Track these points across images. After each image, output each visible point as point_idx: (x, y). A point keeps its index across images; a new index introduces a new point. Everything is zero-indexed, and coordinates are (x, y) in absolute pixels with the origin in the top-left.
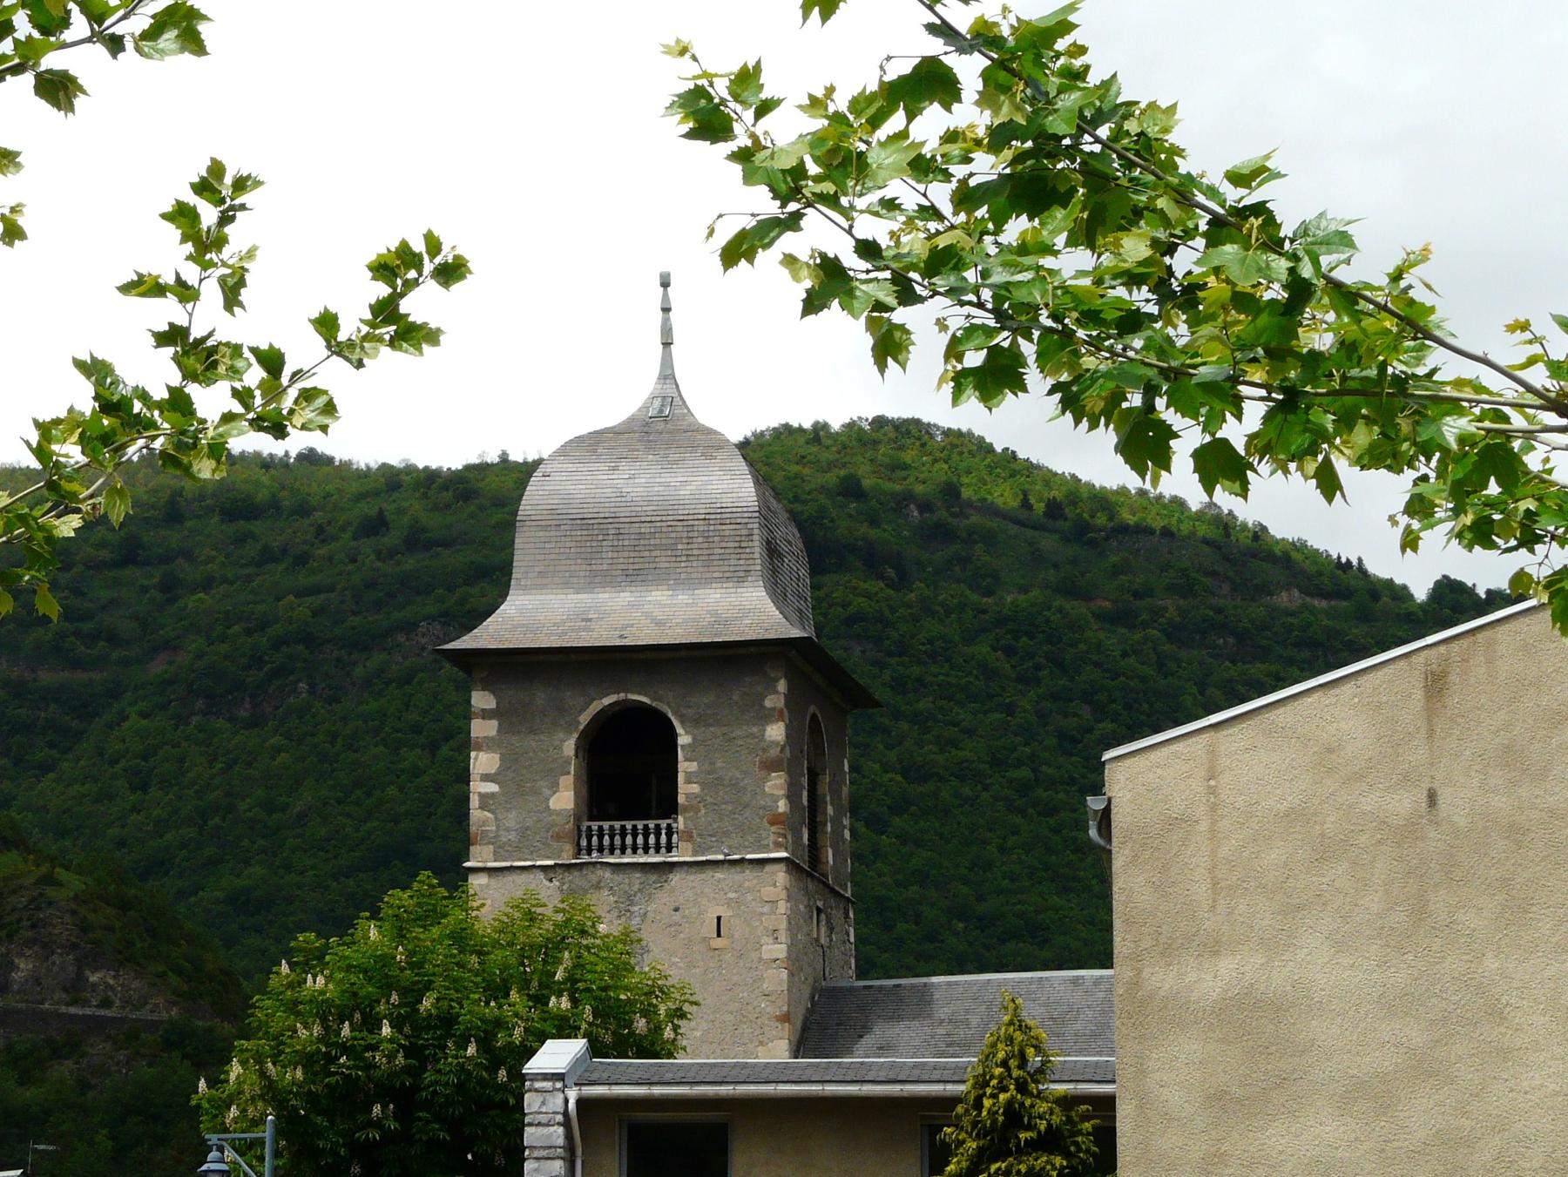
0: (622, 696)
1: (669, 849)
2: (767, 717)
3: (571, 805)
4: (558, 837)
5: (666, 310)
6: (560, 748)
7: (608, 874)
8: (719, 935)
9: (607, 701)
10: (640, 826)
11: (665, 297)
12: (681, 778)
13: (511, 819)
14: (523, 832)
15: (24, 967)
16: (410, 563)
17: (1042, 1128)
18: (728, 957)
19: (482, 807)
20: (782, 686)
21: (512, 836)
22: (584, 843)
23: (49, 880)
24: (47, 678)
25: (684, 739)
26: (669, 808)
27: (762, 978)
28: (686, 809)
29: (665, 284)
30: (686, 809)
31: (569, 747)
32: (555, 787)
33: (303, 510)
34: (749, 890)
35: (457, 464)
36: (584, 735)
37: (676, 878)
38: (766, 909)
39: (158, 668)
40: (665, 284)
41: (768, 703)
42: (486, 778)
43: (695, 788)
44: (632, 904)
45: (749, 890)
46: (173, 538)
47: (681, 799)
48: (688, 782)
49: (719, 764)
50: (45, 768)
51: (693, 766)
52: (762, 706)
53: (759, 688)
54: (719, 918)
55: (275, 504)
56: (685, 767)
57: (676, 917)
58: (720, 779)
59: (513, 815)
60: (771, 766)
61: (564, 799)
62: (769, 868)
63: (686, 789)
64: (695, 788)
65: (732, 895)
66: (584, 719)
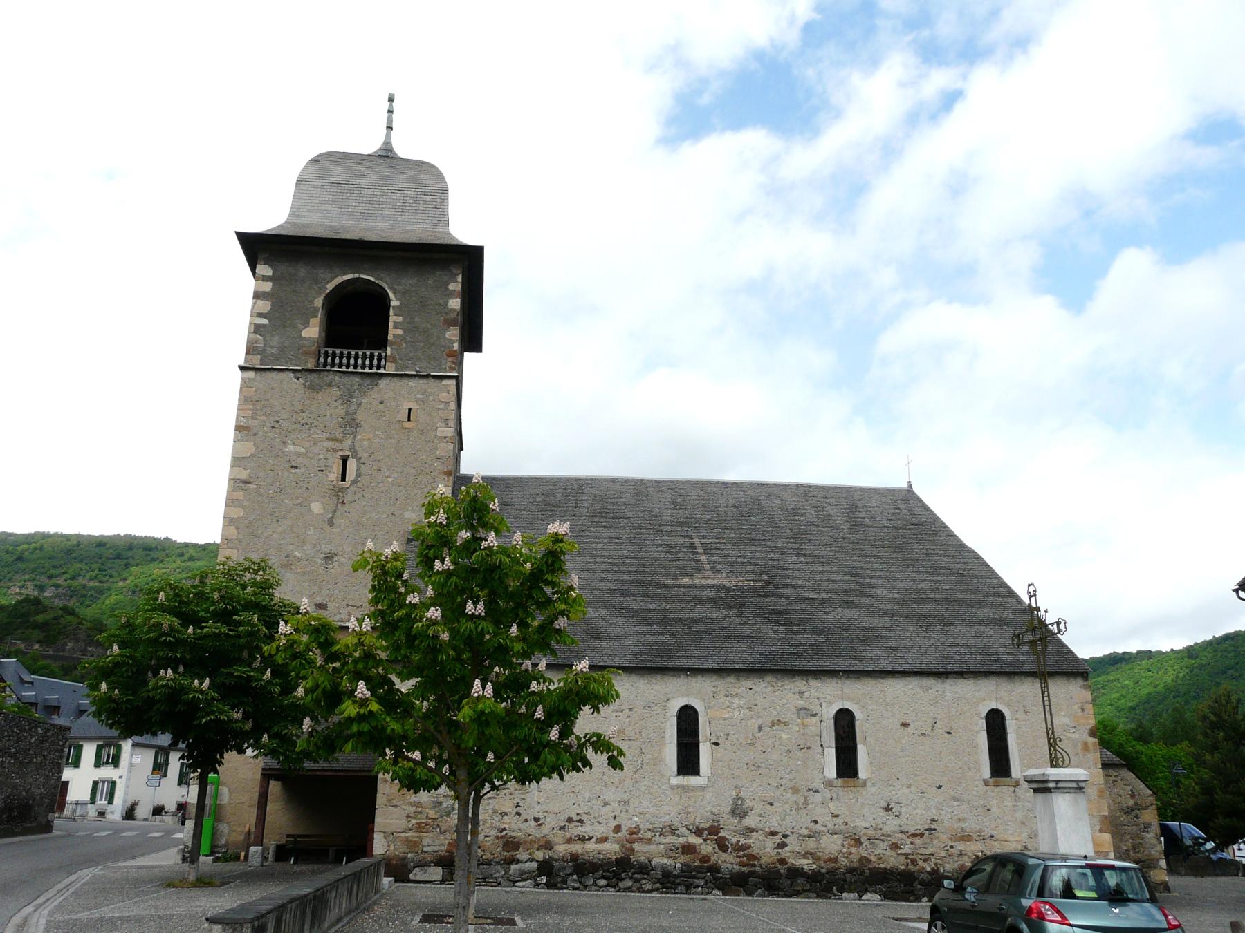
0: (357, 275)
1: (379, 367)
2: (451, 294)
3: (316, 336)
4: (306, 353)
5: (390, 128)
6: (312, 302)
7: (337, 378)
9: (346, 277)
10: (360, 353)
11: (391, 106)
12: (391, 325)
13: (275, 341)
14: (282, 349)
15: (70, 645)
16: (189, 564)
17: (265, 737)
18: (414, 434)
20: (460, 278)
21: (274, 351)
22: (322, 360)
23: (81, 623)
24: (91, 584)
25: (394, 303)
26: (382, 343)
27: (436, 448)
28: (393, 343)
29: (391, 100)
30: (393, 343)
31: (319, 302)
32: (306, 324)
33: (164, 550)
34: (431, 394)
35: (202, 541)
36: (328, 297)
37: (383, 383)
38: (442, 406)
39: (121, 584)
40: (391, 100)
41: (451, 287)
43: (400, 332)
44: (352, 397)
45: (431, 394)
46: (130, 554)
47: (390, 337)
48: (396, 327)
49: (417, 319)
50: (89, 606)
51: (400, 319)
52: (447, 289)
53: (446, 278)
55: (157, 548)
56: (393, 319)
57: (381, 407)
58: (417, 328)
59: (276, 338)
60: (450, 323)
61: (313, 331)
62: (445, 382)
63: (393, 332)
64: (400, 332)
65: (420, 396)
66: (330, 286)
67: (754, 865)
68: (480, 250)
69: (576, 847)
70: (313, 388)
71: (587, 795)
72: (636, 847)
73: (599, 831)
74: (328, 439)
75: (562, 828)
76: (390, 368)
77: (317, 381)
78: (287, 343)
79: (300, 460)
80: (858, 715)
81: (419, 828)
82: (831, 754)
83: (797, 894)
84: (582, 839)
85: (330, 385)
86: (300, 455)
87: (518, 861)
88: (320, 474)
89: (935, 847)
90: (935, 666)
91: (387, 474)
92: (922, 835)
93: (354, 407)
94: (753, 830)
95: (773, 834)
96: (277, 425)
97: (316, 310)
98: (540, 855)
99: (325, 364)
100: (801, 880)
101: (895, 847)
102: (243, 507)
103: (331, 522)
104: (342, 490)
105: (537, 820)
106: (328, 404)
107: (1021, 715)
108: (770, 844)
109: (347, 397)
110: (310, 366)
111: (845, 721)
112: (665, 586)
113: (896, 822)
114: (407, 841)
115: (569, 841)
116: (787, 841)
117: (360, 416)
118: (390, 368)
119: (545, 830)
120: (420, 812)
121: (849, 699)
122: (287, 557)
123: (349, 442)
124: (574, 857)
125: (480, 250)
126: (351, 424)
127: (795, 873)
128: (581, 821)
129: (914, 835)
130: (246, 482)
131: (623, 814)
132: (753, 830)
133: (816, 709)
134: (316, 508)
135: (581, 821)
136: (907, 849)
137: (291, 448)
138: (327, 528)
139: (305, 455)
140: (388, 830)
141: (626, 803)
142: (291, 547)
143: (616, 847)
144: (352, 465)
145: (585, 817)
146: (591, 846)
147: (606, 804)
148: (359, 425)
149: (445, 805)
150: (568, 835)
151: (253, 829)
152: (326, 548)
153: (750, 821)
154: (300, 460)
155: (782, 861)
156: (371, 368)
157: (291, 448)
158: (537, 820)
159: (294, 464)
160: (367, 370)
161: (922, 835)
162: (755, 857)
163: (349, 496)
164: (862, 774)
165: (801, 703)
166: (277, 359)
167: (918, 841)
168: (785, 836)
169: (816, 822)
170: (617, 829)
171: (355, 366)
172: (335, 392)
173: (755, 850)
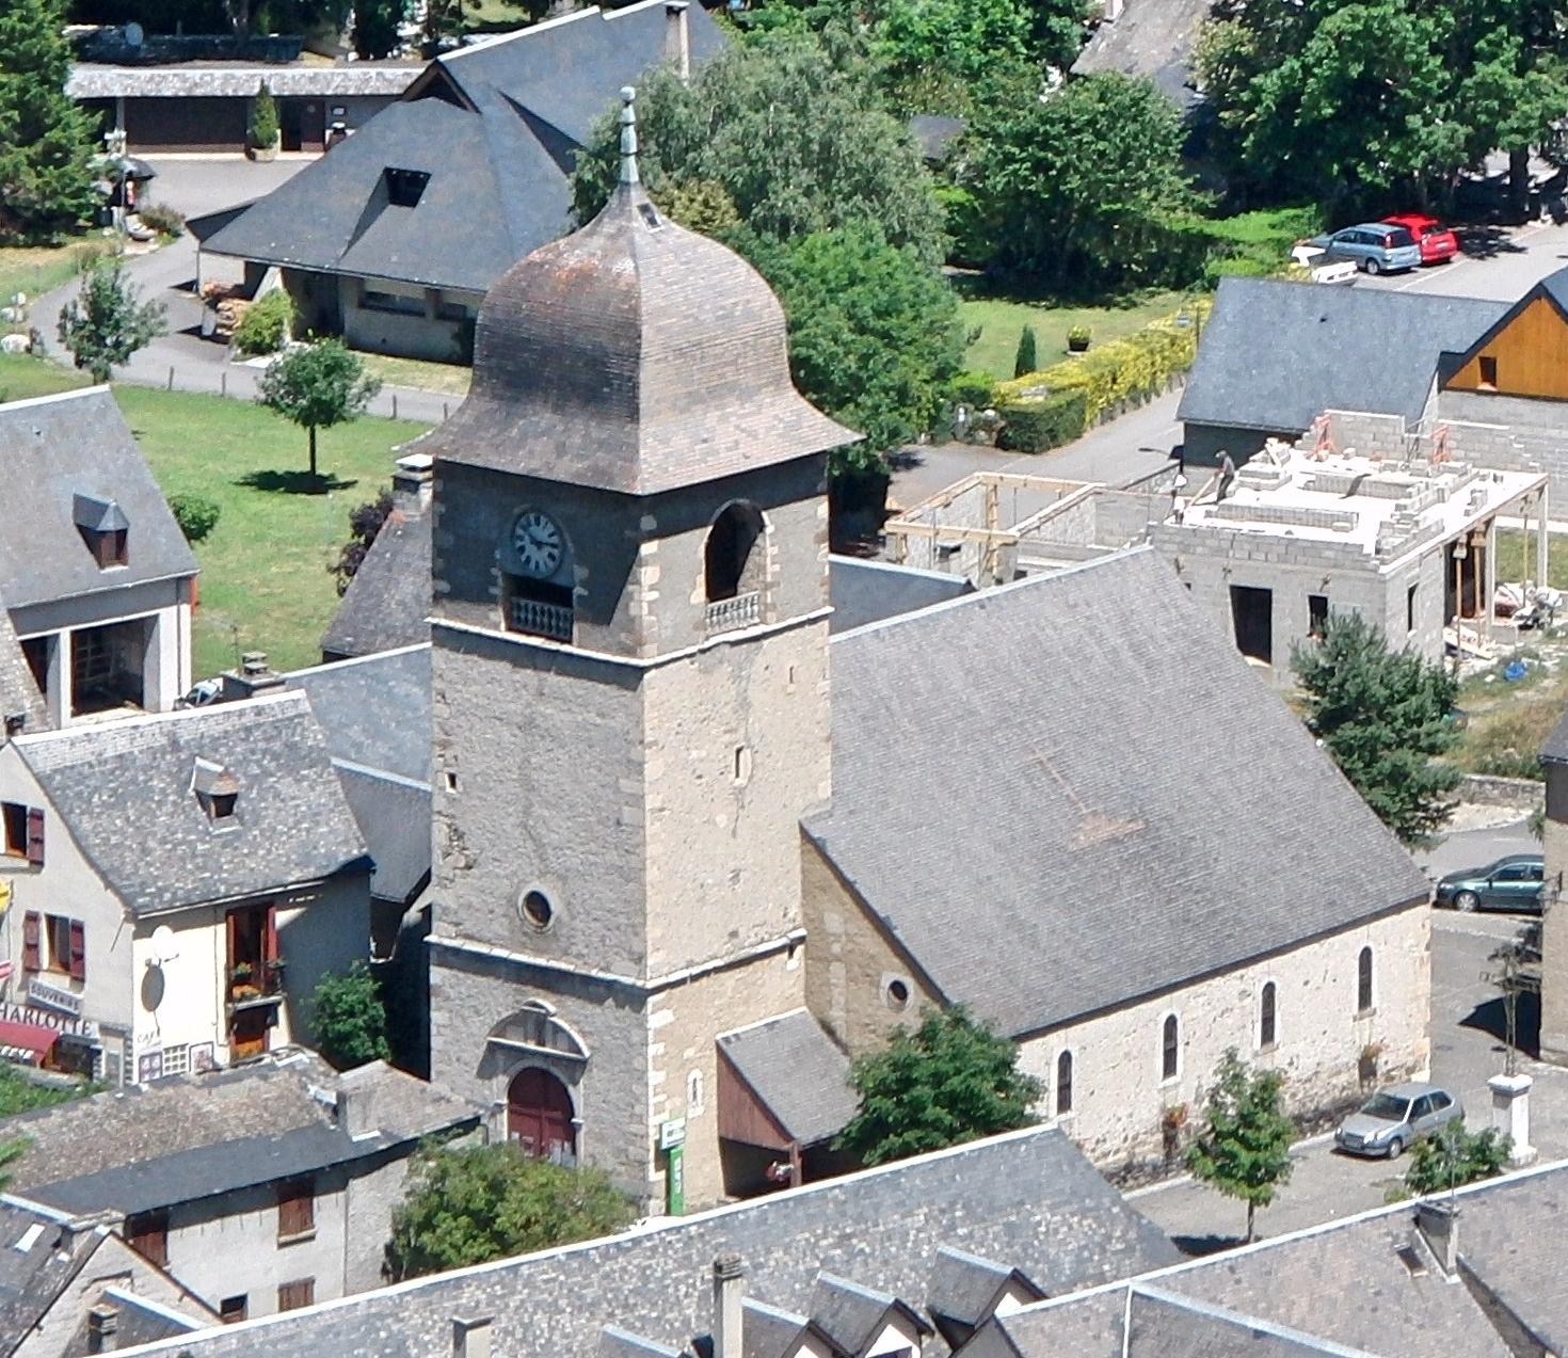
51: (775, 550)
68: (1268, 592)
72: (1137, 1150)
73: (1117, 1143)
74: (726, 732)
80: (1278, 986)
82: (1259, 1026)
84: (1106, 1155)
89: (1318, 1088)
90: (1323, 920)
103: (734, 833)
104: (741, 790)
107: (1382, 947)
125: (1268, 592)
134: (722, 820)
138: (732, 841)
151: (571, 1089)
157: (694, 754)
159: (698, 773)
165: (1242, 987)
167: (1308, 1085)
172: (727, 668)
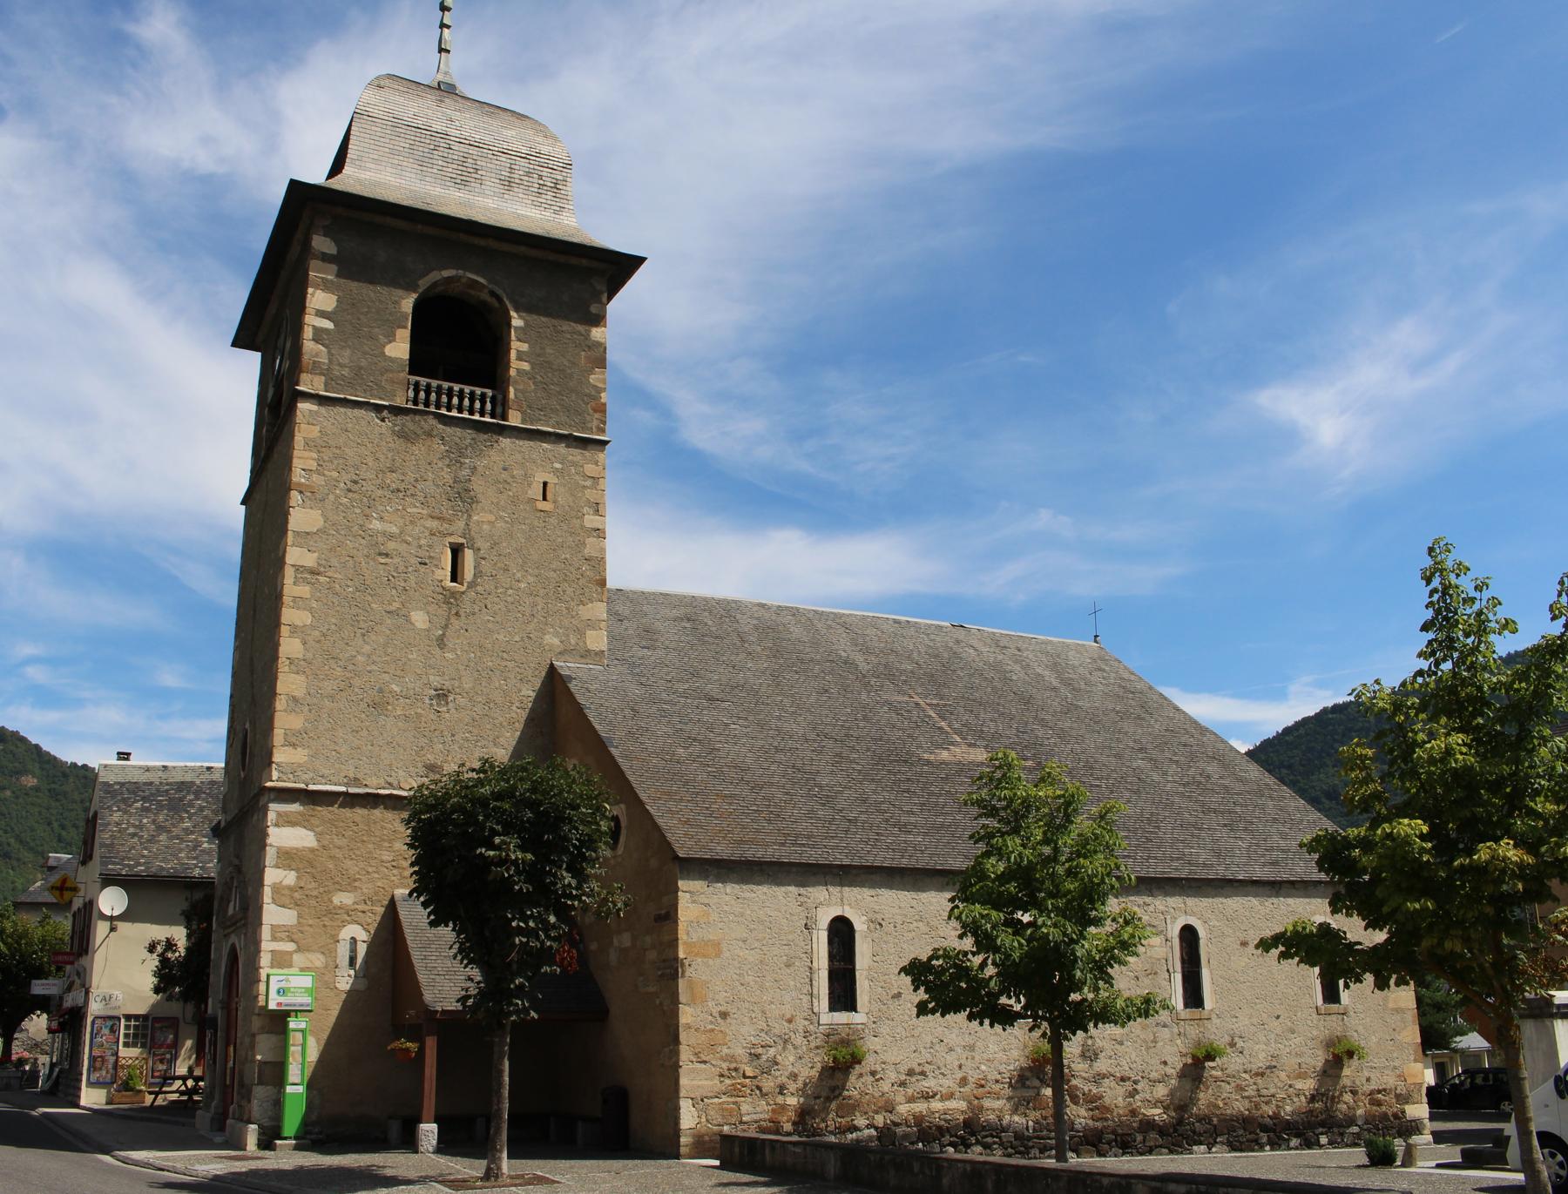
8: (545, 498)
13: (345, 356)
14: (358, 371)
19: (274, 939)
21: (345, 372)
32: (391, 338)
38: (588, 483)
42: (321, 314)
43: (526, 366)
44: (462, 455)
47: (513, 372)
48: (519, 358)
51: (525, 347)
54: (545, 484)
57: (505, 475)
59: (347, 353)
61: (400, 348)
63: (517, 366)
64: (526, 366)
65: (558, 466)
67: (1106, 1119)
69: (920, 1107)
70: (403, 435)
71: (929, 1039)
73: (948, 1083)
75: (903, 1084)
76: (514, 419)
77: (410, 425)
78: (363, 363)
79: (391, 545)
80: (1202, 933)
81: (735, 1092)
83: (1150, 1152)
84: (927, 1096)
85: (429, 435)
86: (391, 537)
87: (856, 1129)
88: (422, 569)
91: (519, 575)
92: (1262, 1075)
93: (465, 472)
94: (1104, 1076)
95: (1123, 1079)
96: (355, 488)
97: (405, 316)
98: (879, 1120)
99: (427, 404)
100: (1153, 1135)
101: (1240, 1088)
102: (311, 610)
103: (441, 642)
104: (453, 594)
105: (873, 1073)
106: (429, 457)
108: (1120, 1091)
109: (456, 456)
110: (400, 401)
111: (1189, 936)
112: (928, 763)
113: (1240, 1060)
114: (721, 1109)
115: (911, 1100)
116: (1139, 1087)
117: (477, 485)
118: (514, 419)
119: (885, 1086)
120: (736, 1069)
121: (1193, 914)
122: (381, 691)
123: (461, 524)
124: (919, 1119)
126: (463, 496)
127: (1148, 1125)
128: (923, 1073)
129: (1257, 1074)
130: (313, 572)
131: (969, 1063)
132: (1104, 1076)
133: (1161, 926)
134: (419, 619)
135: (923, 1073)
136: (1251, 1092)
137: (376, 525)
139: (398, 537)
140: (698, 1094)
141: (972, 1048)
142: (386, 677)
143: (963, 1105)
144: (469, 556)
145: (927, 1068)
146: (936, 1105)
147: (951, 1050)
148: (474, 500)
149: (764, 1058)
150: (910, 1091)
152: (436, 681)
153: (1102, 1065)
154: (391, 545)
155: (1133, 1113)
156: (471, 412)
158: (873, 1073)
160: (454, 413)
161: (1262, 1075)
162: (1108, 1109)
163: (466, 606)
164: (1208, 1004)
166: (350, 385)
167: (1259, 1080)
168: (1136, 1082)
169: (1165, 1063)
170: (963, 1081)
171: (438, 406)
173: (1107, 1101)
